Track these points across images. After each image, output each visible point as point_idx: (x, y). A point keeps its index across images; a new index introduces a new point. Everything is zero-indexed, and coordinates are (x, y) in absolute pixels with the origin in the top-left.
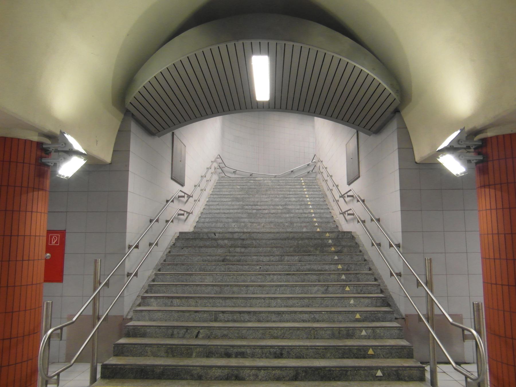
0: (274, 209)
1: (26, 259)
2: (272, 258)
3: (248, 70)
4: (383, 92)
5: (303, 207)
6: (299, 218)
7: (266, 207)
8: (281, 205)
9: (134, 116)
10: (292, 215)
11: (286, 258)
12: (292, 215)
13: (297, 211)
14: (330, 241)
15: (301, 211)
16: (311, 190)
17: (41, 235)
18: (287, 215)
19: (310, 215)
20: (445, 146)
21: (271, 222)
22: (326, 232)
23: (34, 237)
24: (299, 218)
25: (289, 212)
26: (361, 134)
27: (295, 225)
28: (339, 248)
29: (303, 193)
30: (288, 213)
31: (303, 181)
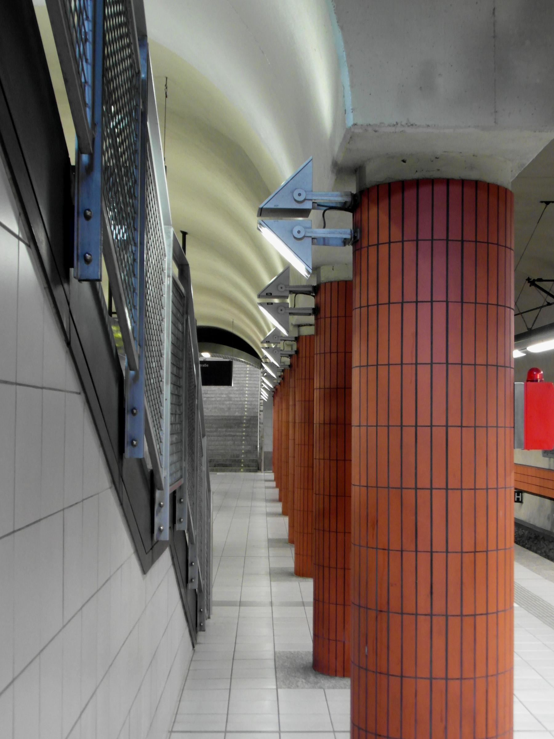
0: (219, 397)
1: (363, 427)
2: (212, 429)
3: (498, 513)
4: (487, 326)
5: (241, 396)
6: (235, 405)
7: (213, 396)
8: (225, 394)
9: (317, 303)
10: (231, 402)
11: (219, 429)
12: (231, 402)
13: (236, 399)
14: (245, 421)
15: (239, 399)
16: (252, 379)
17: (506, 426)
18: (228, 402)
19: (244, 403)
20: (292, 264)
21: (216, 408)
22: (244, 416)
23: (464, 425)
24: (235, 405)
25: (230, 399)
26: (354, 308)
27: (231, 410)
28: (248, 425)
29: (244, 382)
30: (228, 401)
31: (248, 369)
